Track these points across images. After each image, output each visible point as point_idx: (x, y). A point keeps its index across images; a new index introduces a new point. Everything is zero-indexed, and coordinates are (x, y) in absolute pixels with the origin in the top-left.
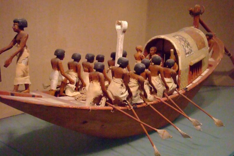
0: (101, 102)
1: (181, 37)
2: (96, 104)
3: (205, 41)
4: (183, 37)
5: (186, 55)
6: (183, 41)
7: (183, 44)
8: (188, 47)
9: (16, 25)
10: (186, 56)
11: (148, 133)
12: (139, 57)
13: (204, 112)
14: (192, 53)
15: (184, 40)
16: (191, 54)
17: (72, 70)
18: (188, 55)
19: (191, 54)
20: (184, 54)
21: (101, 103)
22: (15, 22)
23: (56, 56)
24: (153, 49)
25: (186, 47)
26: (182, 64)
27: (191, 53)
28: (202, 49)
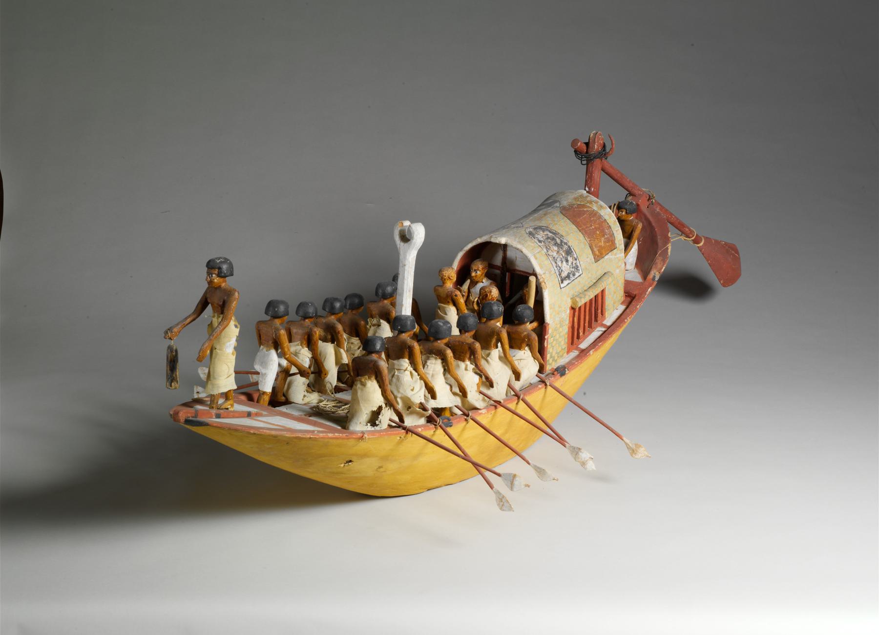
1: (550, 234)
6: (556, 244)
7: (555, 254)
8: (567, 261)
10: (562, 286)
14: (577, 274)
15: (558, 241)
18: (566, 282)
20: (557, 280)
27: (574, 275)
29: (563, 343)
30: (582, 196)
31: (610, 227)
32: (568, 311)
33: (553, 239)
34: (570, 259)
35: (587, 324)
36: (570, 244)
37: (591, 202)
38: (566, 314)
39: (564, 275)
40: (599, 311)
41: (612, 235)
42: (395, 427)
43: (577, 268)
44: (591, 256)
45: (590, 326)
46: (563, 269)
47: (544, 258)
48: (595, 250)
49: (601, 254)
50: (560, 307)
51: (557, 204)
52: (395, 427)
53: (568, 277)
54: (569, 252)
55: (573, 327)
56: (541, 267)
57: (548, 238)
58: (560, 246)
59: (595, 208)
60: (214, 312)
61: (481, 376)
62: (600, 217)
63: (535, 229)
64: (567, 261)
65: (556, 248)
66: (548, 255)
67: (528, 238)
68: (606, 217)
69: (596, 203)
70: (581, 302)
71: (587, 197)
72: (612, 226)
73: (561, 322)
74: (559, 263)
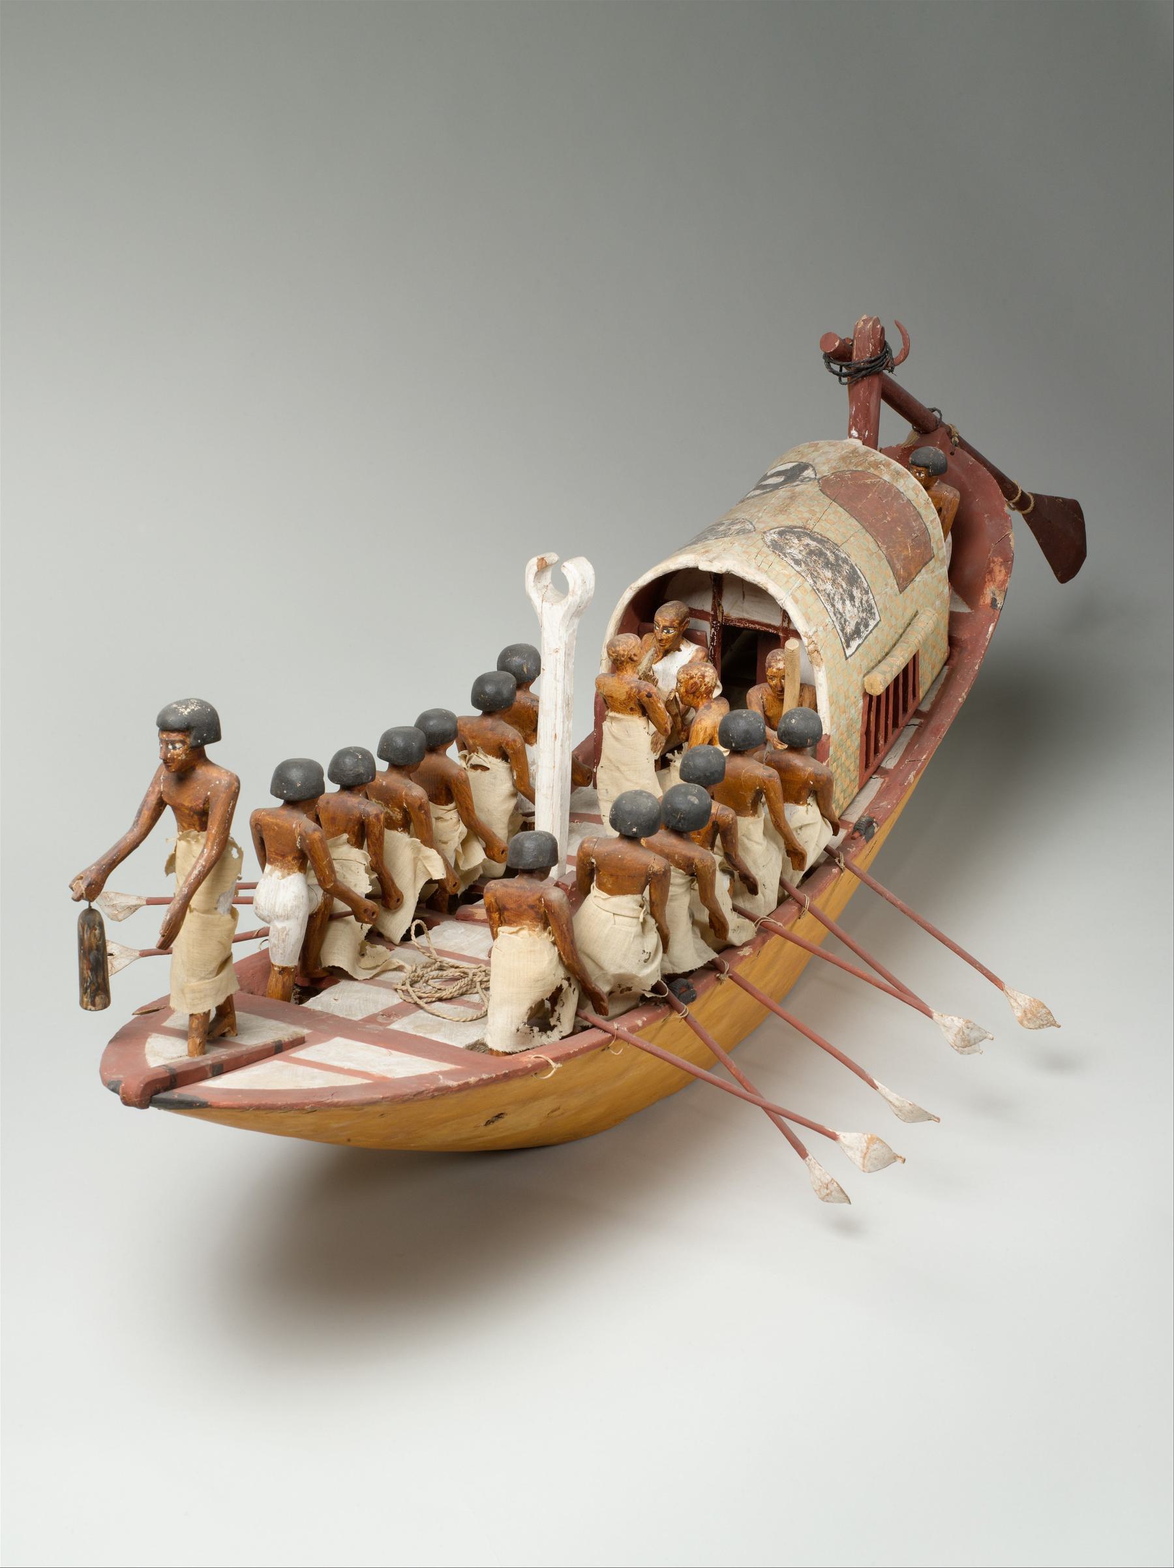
0: (556, 1015)
1: (813, 544)
2: (536, 1029)
3: (930, 528)
4: (822, 541)
5: (848, 646)
6: (827, 564)
7: (828, 587)
8: (852, 598)
9: (178, 745)
10: (849, 652)
11: (708, 1070)
12: (629, 697)
13: (892, 644)
14: (872, 623)
15: (832, 558)
16: (870, 628)
17: (345, 836)
18: (854, 644)
19: (870, 628)
20: (837, 642)
21: (559, 1020)
22: (165, 728)
23: (281, 802)
24: (667, 614)
25: (844, 603)
26: (832, 701)
27: (866, 626)
28: (917, 579)
29: (852, 768)
30: (855, 451)
31: (919, 515)
32: (861, 703)
33: (821, 554)
34: (856, 593)
35: (890, 722)
36: (852, 560)
37: (876, 465)
38: (856, 710)
39: (849, 629)
40: (910, 689)
41: (925, 531)
42: (782, 484)
43: (869, 610)
44: (892, 581)
45: (895, 724)
46: (848, 616)
47: (810, 598)
48: (898, 566)
49: (910, 574)
50: (847, 698)
51: (809, 473)
52: (782, 484)
53: (857, 632)
54: (853, 579)
55: (867, 733)
56: (808, 620)
57: (811, 553)
58: (835, 567)
59: (886, 477)
60: (182, 827)
61: (732, 875)
62: (899, 494)
63: (781, 533)
64: (852, 598)
65: (829, 574)
66: (816, 591)
67: (772, 557)
68: (910, 495)
69: (888, 465)
70: (878, 689)
71: (867, 453)
72: (922, 512)
73: (850, 726)
74: (839, 606)
